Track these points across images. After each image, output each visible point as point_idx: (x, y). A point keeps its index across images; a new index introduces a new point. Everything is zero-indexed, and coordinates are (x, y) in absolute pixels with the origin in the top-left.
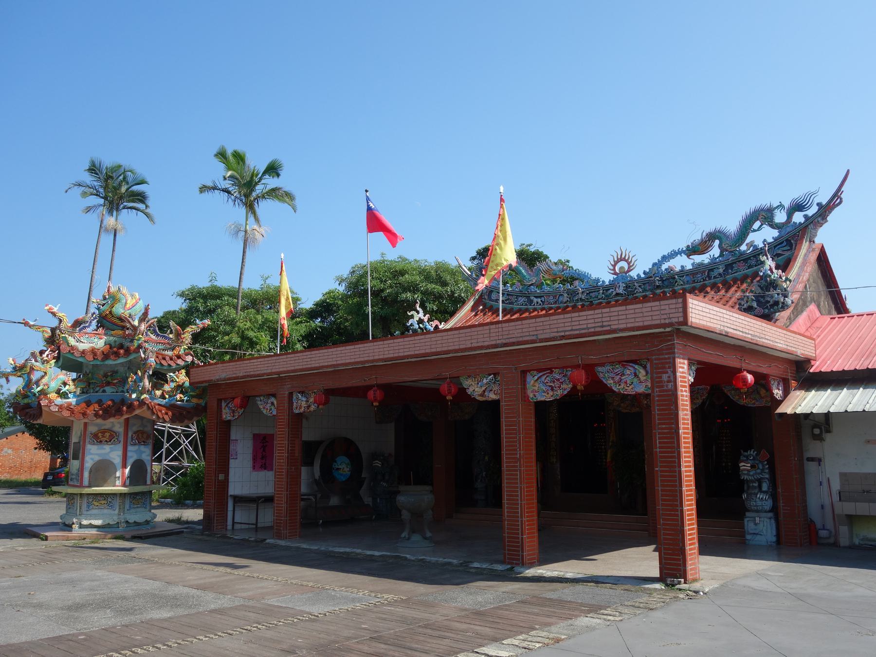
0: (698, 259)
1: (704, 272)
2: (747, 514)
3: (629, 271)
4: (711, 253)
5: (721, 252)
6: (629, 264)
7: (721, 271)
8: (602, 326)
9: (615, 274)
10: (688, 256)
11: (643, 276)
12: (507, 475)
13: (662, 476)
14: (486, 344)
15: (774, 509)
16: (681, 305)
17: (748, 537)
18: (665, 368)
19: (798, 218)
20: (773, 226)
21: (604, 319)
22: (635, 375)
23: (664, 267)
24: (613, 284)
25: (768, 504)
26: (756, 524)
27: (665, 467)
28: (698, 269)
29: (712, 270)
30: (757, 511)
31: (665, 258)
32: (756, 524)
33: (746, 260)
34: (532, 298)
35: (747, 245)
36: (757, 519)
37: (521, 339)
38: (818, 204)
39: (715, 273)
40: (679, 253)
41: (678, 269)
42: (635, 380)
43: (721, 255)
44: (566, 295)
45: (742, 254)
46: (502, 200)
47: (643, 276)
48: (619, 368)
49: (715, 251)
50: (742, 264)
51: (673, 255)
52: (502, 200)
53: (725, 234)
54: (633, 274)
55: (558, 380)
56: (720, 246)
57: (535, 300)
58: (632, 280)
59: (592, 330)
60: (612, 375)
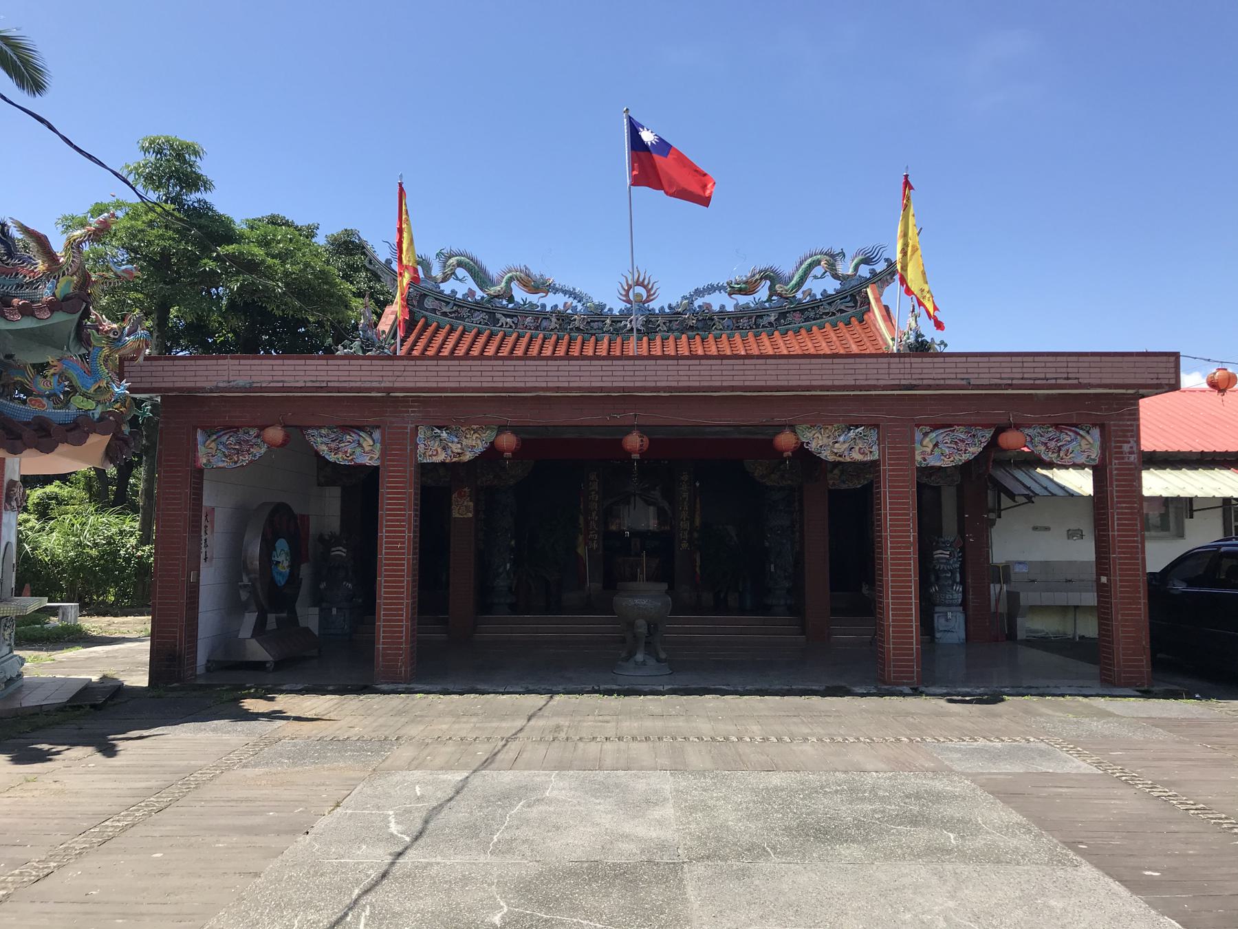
0: (743, 300)
1: (751, 318)
2: (937, 609)
3: (648, 301)
4: (757, 296)
5: (770, 296)
6: (648, 291)
7: (772, 319)
8: (1068, 379)
9: (629, 301)
10: (730, 295)
11: (667, 310)
12: (892, 565)
13: (1121, 564)
14: (882, 383)
15: (964, 604)
16: (1172, 365)
17: (938, 635)
18: (1125, 436)
19: (864, 271)
20: (836, 276)
21: (1070, 370)
22: (360, 445)
23: (698, 302)
24: (626, 314)
25: (958, 597)
26: (947, 620)
27: (1124, 553)
28: (742, 312)
29: (761, 317)
30: (949, 605)
31: (698, 293)
32: (947, 620)
33: (802, 311)
34: (498, 316)
35: (804, 292)
36: (949, 614)
37: (942, 382)
38: (886, 260)
39: (765, 321)
40: (720, 288)
41: (716, 308)
42: (359, 450)
43: (769, 300)
44: (554, 320)
45: (800, 302)
46: (907, 184)
47: (667, 310)
48: (1052, 432)
49: (763, 293)
50: (797, 314)
51: (711, 289)
52: (907, 184)
53: (777, 275)
54: (655, 305)
55: (963, 441)
56: (770, 288)
57: (503, 320)
58: (651, 312)
59: (1053, 382)
60: (1043, 439)
